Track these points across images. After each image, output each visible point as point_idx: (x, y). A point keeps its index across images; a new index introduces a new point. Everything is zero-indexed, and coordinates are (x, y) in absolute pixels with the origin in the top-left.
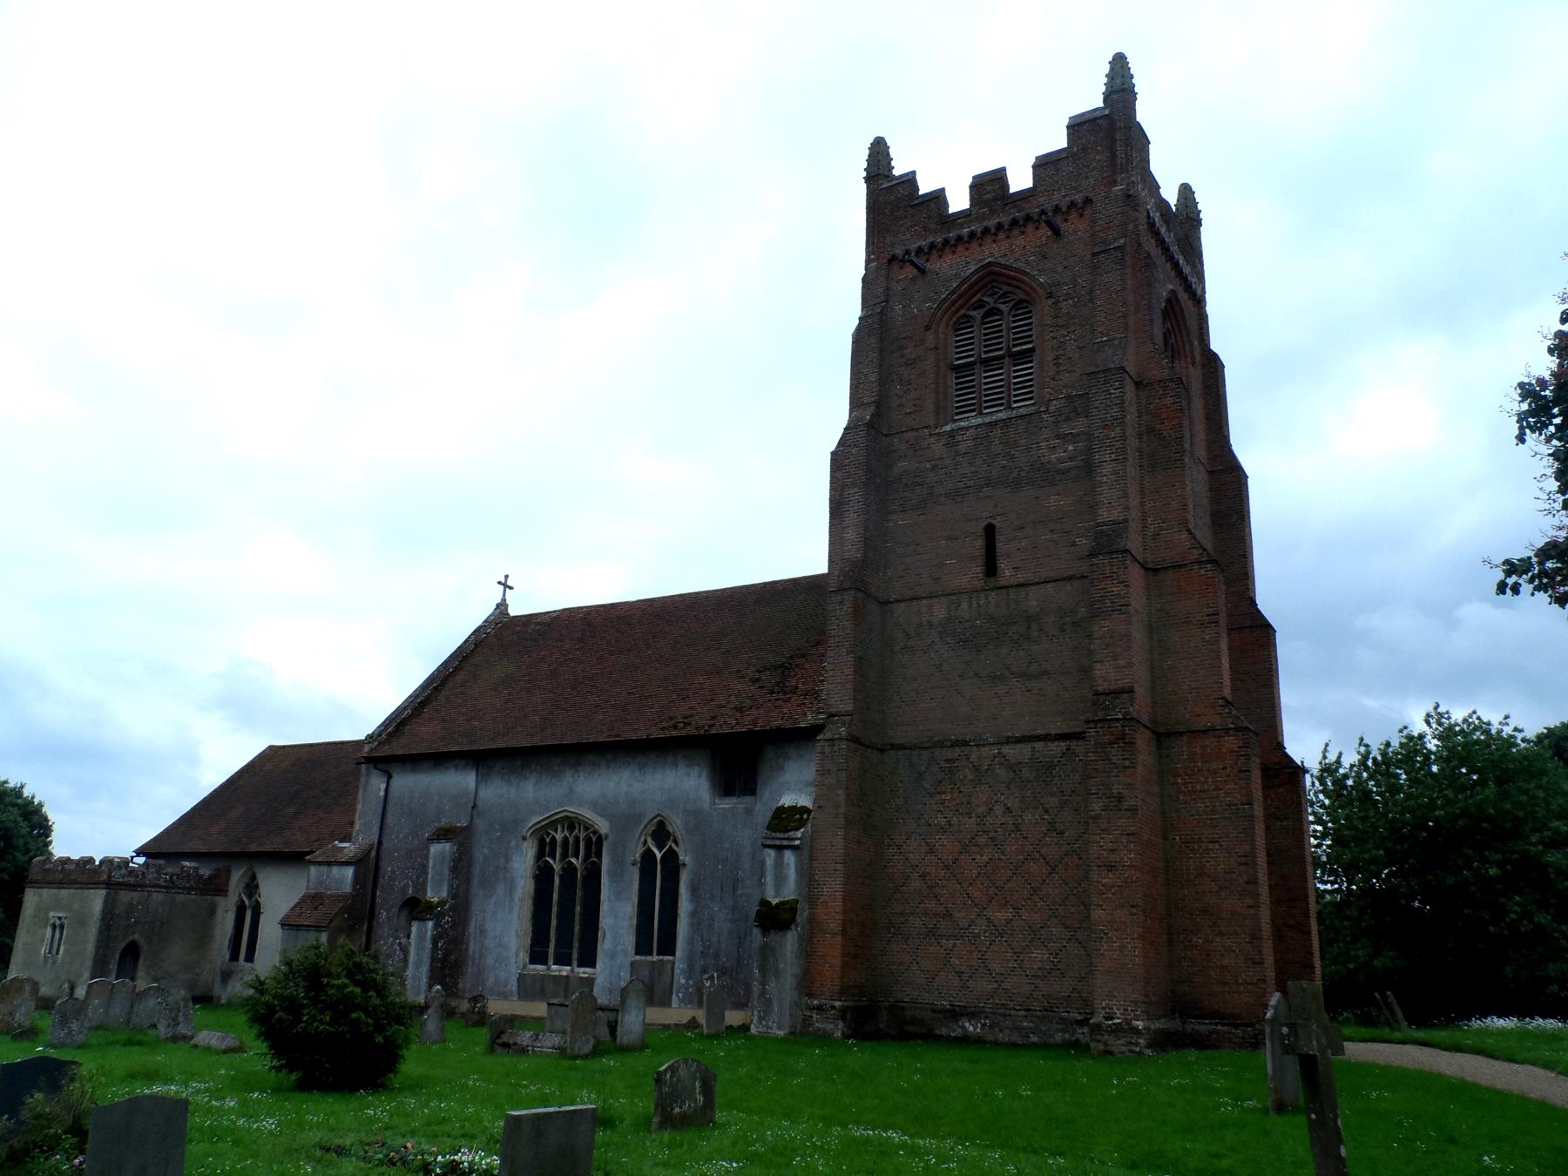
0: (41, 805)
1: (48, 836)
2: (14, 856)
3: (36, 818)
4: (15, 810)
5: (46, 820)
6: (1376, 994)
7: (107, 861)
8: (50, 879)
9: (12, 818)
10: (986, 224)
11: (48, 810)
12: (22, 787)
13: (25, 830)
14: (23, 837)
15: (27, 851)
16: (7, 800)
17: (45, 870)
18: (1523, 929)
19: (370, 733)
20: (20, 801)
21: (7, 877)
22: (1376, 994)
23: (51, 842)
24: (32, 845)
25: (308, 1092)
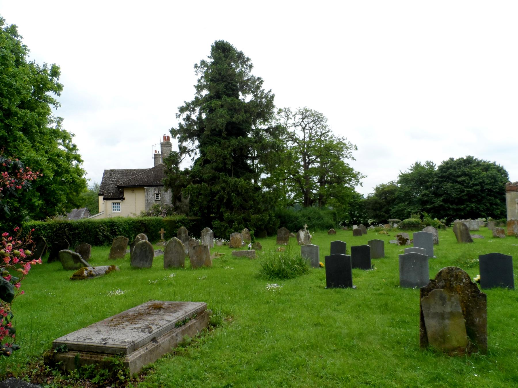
0: (503, 167)
1: (507, 176)
2: (498, 184)
3: (502, 171)
4: (495, 170)
5: (505, 171)
6: (212, 215)
7: (404, 179)
8: (513, 189)
9: (494, 172)
10: (233, 261)
11: (505, 168)
12: (495, 162)
13: (500, 176)
14: (499, 177)
15: (502, 182)
16: (491, 167)
17: (511, 186)
18: (478, 260)
19: (67, 131)
20: (495, 167)
21: (498, 190)
22: (212, 215)
23: (509, 178)
24: (503, 180)
25: (172, 196)
